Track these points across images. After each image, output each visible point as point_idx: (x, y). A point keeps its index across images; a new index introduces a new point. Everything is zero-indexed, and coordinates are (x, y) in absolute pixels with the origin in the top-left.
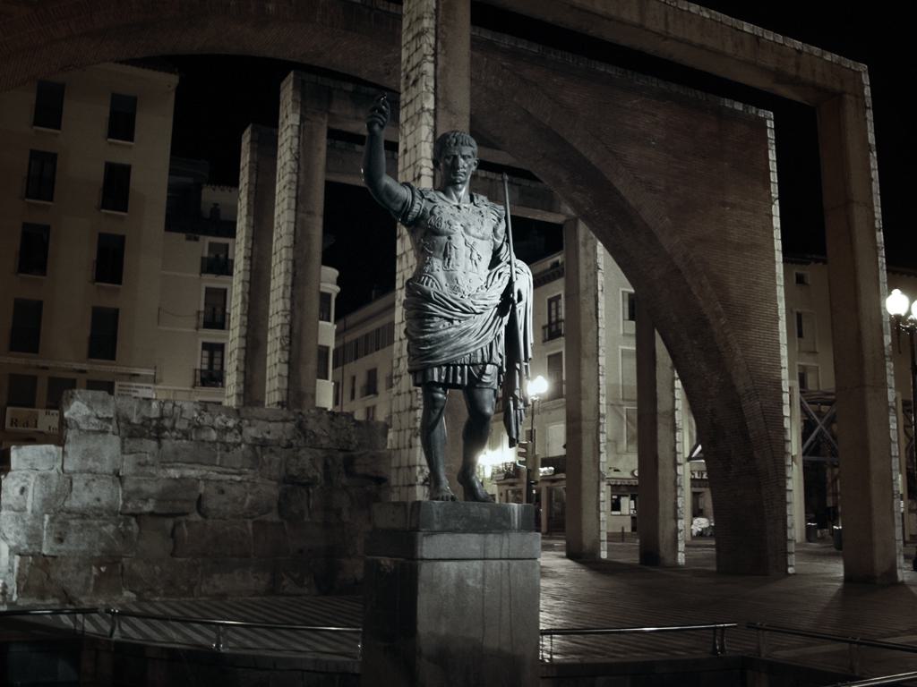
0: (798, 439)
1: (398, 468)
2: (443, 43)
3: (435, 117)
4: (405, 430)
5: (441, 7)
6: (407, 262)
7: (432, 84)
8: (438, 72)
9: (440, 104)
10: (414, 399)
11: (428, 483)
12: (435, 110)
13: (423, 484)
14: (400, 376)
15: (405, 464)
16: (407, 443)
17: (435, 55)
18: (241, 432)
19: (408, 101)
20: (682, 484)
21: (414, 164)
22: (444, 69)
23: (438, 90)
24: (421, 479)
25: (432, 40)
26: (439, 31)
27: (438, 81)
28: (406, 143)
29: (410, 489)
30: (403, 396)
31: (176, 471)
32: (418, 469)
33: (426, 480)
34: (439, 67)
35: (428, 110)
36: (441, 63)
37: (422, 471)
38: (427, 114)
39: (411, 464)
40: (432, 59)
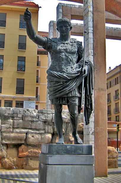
9: (95, 9)
12: (93, 11)
13: (92, 134)
23: (94, 4)
24: (91, 133)
29: (88, 135)
32: (90, 129)
33: (93, 133)
35: (91, 11)
39: (88, 127)
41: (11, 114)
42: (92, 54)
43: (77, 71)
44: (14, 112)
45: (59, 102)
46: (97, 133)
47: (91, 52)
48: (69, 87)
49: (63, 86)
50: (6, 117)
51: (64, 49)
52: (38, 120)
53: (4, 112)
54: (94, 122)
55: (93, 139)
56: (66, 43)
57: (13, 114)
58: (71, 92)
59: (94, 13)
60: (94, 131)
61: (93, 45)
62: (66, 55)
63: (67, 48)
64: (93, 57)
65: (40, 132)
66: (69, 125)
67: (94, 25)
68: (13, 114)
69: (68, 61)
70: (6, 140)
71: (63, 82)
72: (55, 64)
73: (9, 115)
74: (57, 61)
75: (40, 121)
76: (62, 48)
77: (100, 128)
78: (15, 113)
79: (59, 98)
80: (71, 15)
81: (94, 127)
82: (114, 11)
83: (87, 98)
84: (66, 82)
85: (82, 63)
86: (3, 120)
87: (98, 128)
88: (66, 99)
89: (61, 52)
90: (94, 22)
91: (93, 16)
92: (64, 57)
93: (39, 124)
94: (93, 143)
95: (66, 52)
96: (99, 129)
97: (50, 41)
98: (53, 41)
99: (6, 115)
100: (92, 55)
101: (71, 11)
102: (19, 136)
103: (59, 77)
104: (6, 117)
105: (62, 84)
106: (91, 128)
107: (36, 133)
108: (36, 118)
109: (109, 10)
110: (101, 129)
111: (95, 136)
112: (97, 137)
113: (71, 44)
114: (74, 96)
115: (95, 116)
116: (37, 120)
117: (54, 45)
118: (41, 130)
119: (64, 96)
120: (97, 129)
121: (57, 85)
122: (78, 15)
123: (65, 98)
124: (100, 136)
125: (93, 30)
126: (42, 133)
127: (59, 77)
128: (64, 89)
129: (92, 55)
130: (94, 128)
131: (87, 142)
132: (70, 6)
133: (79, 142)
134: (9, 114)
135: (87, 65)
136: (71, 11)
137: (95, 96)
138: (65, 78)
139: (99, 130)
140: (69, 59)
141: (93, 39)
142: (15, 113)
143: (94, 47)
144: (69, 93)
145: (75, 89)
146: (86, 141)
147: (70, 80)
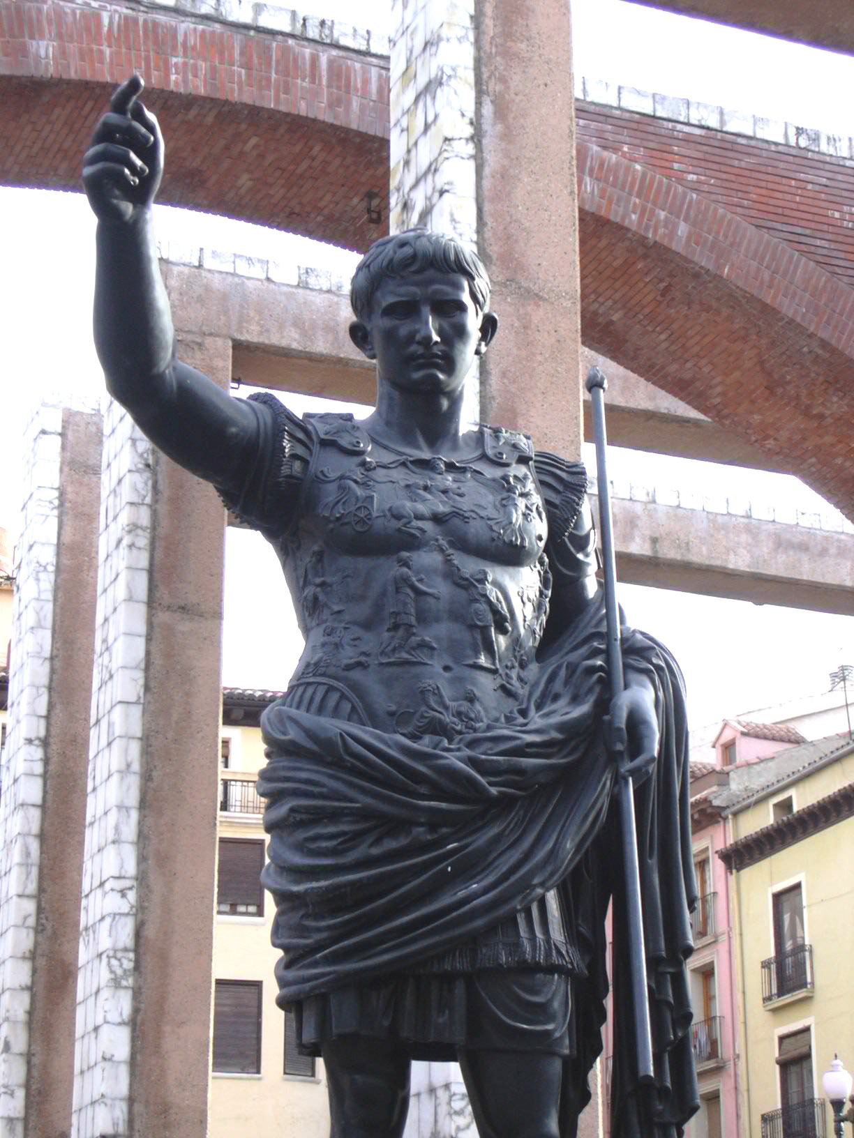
2: (501, 112)
8: (486, 183)
17: (477, 138)
27: (487, 207)
34: (487, 171)
43: (561, 727)
48: (491, 879)
51: (437, 519)
56: (451, 467)
62: (451, 574)
63: (465, 504)
69: (472, 627)
71: (433, 827)
72: (348, 655)
74: (368, 625)
76: (422, 508)
80: (238, 346)
82: (611, 323)
84: (463, 825)
85: (595, 653)
89: (412, 542)
90: (494, 381)
92: (441, 588)
95: (452, 544)
97: (301, 435)
98: (325, 443)
113: (491, 472)
117: (333, 475)
122: (294, 345)
123: (448, 979)
128: (446, 900)
138: (452, 785)
140: (483, 607)
144: (491, 929)
147: (504, 804)
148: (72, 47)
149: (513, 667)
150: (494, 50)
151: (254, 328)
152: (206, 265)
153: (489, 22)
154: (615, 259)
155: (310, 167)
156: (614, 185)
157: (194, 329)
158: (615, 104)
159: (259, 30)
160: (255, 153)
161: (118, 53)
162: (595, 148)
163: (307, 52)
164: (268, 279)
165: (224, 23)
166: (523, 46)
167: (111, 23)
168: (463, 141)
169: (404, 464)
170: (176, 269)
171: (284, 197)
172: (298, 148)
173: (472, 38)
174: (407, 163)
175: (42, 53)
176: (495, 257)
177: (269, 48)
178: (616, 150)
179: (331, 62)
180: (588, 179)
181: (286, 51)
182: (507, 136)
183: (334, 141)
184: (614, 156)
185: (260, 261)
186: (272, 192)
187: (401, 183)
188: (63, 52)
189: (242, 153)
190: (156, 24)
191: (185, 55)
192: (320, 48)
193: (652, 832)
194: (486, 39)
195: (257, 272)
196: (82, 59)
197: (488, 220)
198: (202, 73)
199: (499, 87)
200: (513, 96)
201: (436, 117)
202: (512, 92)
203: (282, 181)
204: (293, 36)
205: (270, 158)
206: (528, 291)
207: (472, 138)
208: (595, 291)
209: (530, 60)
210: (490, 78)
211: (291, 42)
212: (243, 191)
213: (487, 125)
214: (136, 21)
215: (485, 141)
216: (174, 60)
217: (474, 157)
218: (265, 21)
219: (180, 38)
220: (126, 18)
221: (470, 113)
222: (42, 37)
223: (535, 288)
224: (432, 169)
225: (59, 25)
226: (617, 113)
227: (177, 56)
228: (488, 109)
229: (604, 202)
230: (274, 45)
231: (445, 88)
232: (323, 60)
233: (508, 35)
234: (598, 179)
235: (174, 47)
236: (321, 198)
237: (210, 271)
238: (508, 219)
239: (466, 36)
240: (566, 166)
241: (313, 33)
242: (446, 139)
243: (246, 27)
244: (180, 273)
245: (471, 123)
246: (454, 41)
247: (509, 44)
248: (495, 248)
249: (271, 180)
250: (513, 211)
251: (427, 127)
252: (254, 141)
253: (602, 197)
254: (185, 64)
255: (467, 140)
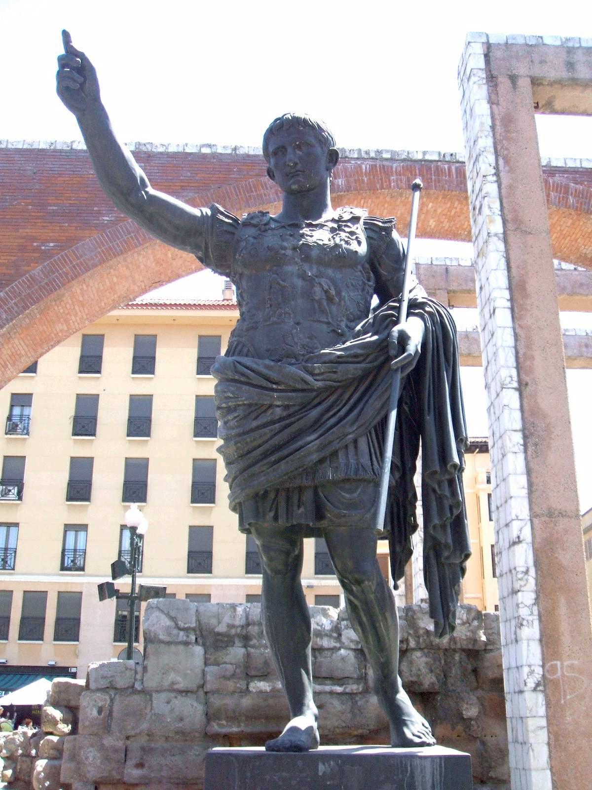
0: (402, 753)
1: (508, 669)
2: (507, 162)
3: (506, 241)
4: (510, 620)
5: (498, 123)
6: (495, 413)
7: (497, 206)
8: (503, 191)
9: (510, 226)
10: (515, 578)
11: (541, 688)
12: (505, 233)
13: (535, 690)
14: (501, 553)
15: (513, 665)
16: (513, 637)
17: (497, 174)
18: (340, 635)
19: (477, 234)
20: (69, 141)
21: (488, 299)
22: (510, 187)
23: (506, 211)
24: (531, 684)
25: (492, 158)
26: (499, 147)
27: (504, 201)
28: (480, 280)
29: (520, 696)
30: (505, 576)
31: (267, 684)
32: (526, 670)
33: (538, 685)
34: (503, 186)
35: (496, 235)
36: (505, 182)
37: (532, 672)
38: (495, 239)
39: (519, 664)
40: (495, 178)
41: (238, 627)
42: (515, 385)
44: (250, 617)
45: (276, 518)
46: (556, 683)
47: (511, 377)
49: (292, 423)
50: (220, 637)
52: (338, 645)
53: (213, 621)
54: (541, 641)
55: (542, 711)
57: (248, 625)
58: (335, 454)
59: (511, 239)
60: (543, 676)
61: (517, 353)
64: (517, 394)
65: (348, 690)
66: (454, 659)
67: (514, 282)
68: (248, 625)
70: (224, 722)
73: (233, 632)
75: (346, 648)
77: (566, 663)
78: (254, 624)
79: (272, 496)
81: (541, 663)
83: (434, 491)
86: (212, 650)
87: (559, 663)
88: (308, 496)
90: (514, 271)
91: (507, 251)
93: (343, 659)
94: (542, 728)
96: (562, 668)
99: (222, 628)
100: (515, 389)
101: (447, 277)
102: (225, 704)
103: (264, 383)
104: (220, 637)
105: (281, 419)
106: (530, 666)
107: (331, 693)
108: (330, 636)
109: (572, 257)
110: (572, 667)
111: (546, 696)
112: (559, 700)
114: (353, 476)
115: (543, 618)
116: (333, 644)
118: (351, 681)
119: (298, 482)
120: (554, 669)
121: (255, 424)
124: (568, 697)
125: (511, 300)
126: (356, 694)
127: (264, 383)
129: (515, 389)
130: (543, 666)
131: (520, 721)
132: (443, 263)
133: (409, 735)
134: (233, 626)
135: (421, 316)
136: (447, 277)
137: (538, 540)
139: (563, 675)
141: (514, 329)
142: (254, 624)
143: (521, 360)
144: (321, 461)
145: (355, 441)
146: (514, 721)
148: (352, 180)
149: (342, 321)
150: (502, 138)
151: (455, 284)
152: (434, 263)
153: (499, 129)
154: (588, 228)
155: (456, 212)
156: (582, 198)
157: (431, 287)
158: (579, 166)
159: (425, 161)
160: (432, 210)
161: (370, 179)
162: (573, 185)
163: (446, 166)
164: (459, 265)
165: (412, 161)
166: (514, 135)
167: (366, 168)
168: (491, 176)
169: (283, 227)
170: (422, 266)
171: (449, 226)
172: (448, 205)
173: (491, 135)
174: (473, 191)
175: (340, 184)
176: (509, 219)
177: (430, 168)
178: (581, 184)
179: (456, 169)
180: (570, 197)
181: (437, 167)
182: (511, 171)
183: (462, 199)
184: (581, 187)
185: (455, 258)
186: (444, 225)
187: (472, 200)
188: (348, 181)
189: (427, 211)
190: (384, 166)
191: (397, 175)
192: (451, 164)
193: (429, 402)
194: (498, 135)
195: (455, 263)
196: (356, 183)
197: (505, 205)
198: (404, 181)
199: (506, 152)
200: (511, 155)
201: (480, 169)
202: (512, 153)
203: (447, 220)
204: (440, 161)
205: (439, 211)
206: (526, 232)
207: (495, 174)
208: (583, 244)
209: (518, 139)
210: (501, 149)
211: (439, 163)
212: (432, 227)
213: (501, 167)
214: (376, 166)
215: (501, 174)
216: (392, 178)
217: (497, 181)
218: (428, 157)
219: (394, 170)
220: (372, 165)
221: (493, 164)
222: (339, 178)
223: (529, 230)
224: (481, 190)
225: (346, 173)
226: (581, 169)
227: (393, 176)
228: (501, 162)
229: (579, 205)
230: (433, 165)
231: (481, 156)
232: (453, 168)
233: (507, 131)
234: (575, 196)
235: (392, 172)
236: (464, 225)
237: (435, 265)
238: (514, 204)
239: (488, 135)
240: (538, 179)
241: (448, 158)
242: (484, 176)
243: (421, 161)
244: (424, 268)
245: (494, 168)
246: (484, 137)
247: (508, 135)
248: (509, 216)
249: (442, 220)
250: (516, 200)
251: (478, 174)
252: (431, 205)
253: (578, 203)
254: (397, 179)
255: (493, 175)
